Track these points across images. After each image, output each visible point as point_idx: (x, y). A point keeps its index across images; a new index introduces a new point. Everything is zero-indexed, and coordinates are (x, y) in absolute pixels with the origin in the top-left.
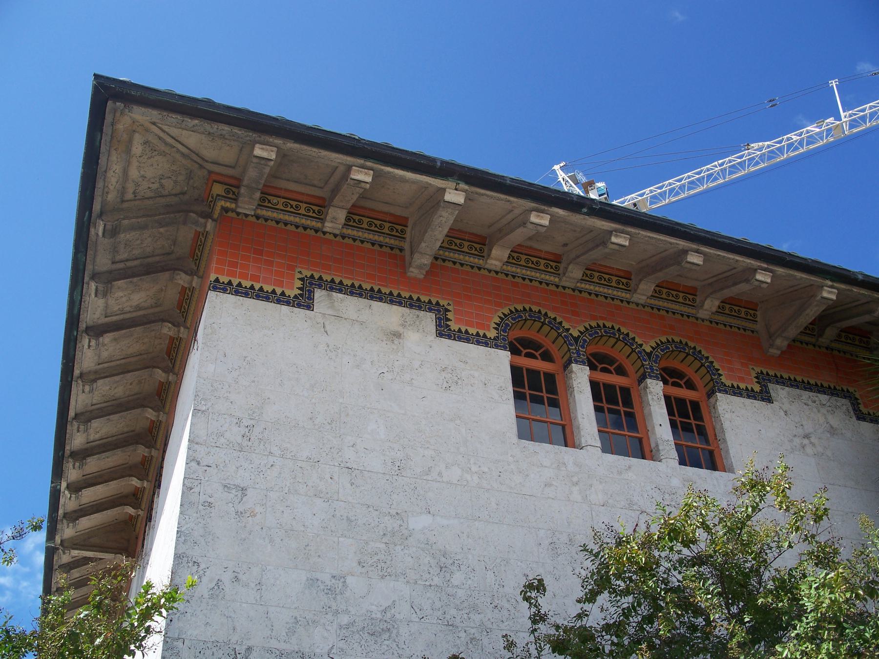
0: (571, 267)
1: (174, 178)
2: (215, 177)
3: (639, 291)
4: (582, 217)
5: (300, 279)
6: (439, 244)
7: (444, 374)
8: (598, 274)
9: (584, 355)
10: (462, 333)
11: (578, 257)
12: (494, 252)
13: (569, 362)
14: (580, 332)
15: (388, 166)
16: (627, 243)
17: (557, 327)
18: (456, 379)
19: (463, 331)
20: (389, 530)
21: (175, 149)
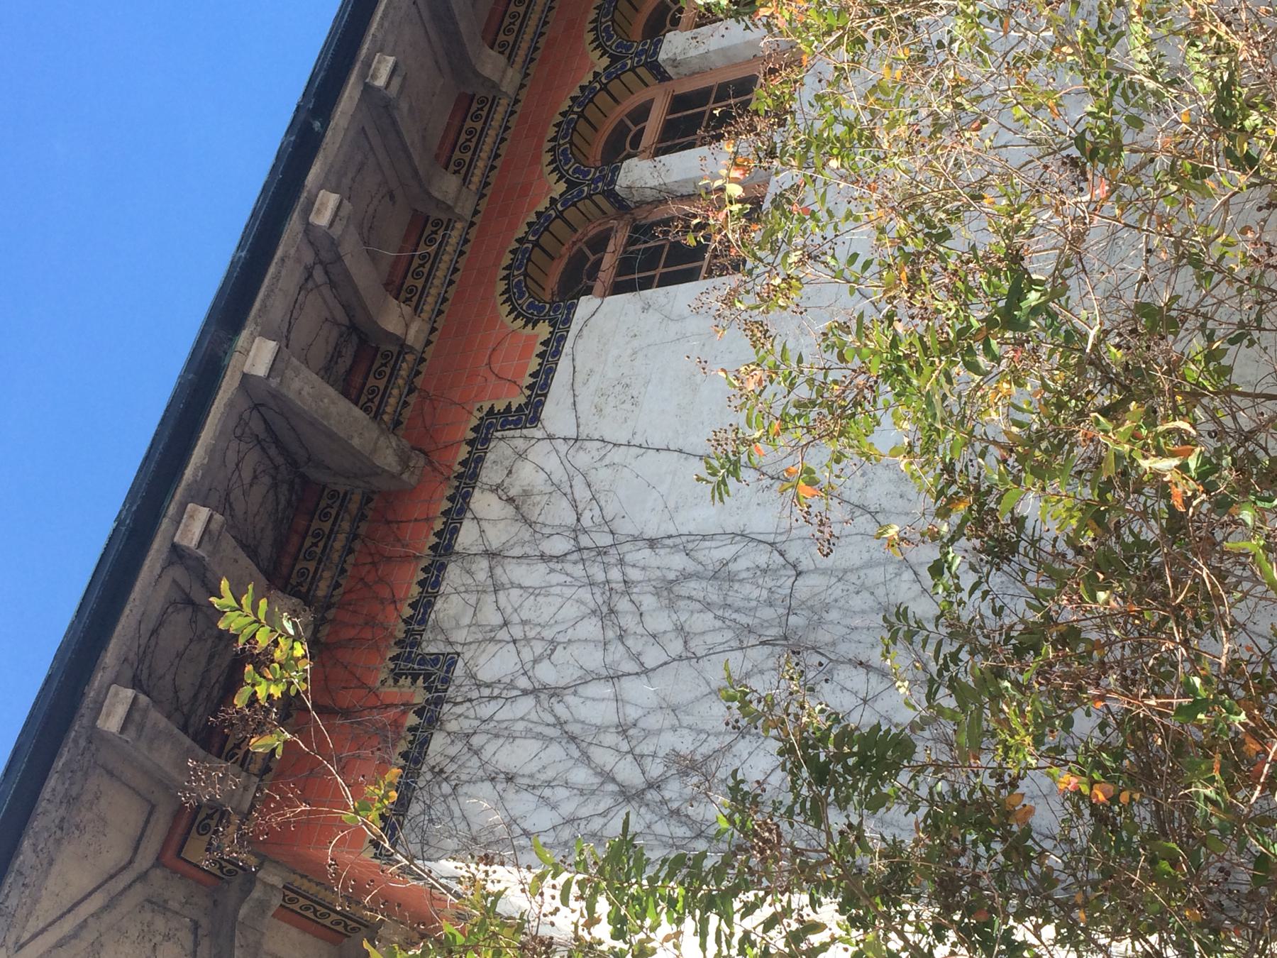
0: (436, 194)
1: (158, 938)
2: (170, 853)
3: (495, 78)
4: (329, 133)
5: (396, 681)
6: (357, 412)
7: (608, 410)
8: (457, 152)
10: (535, 383)
11: (416, 172)
12: (390, 328)
13: (611, 195)
15: (183, 474)
16: (391, 60)
17: (546, 220)
18: (619, 388)
19: (532, 380)
20: (893, 489)
21: (91, 920)
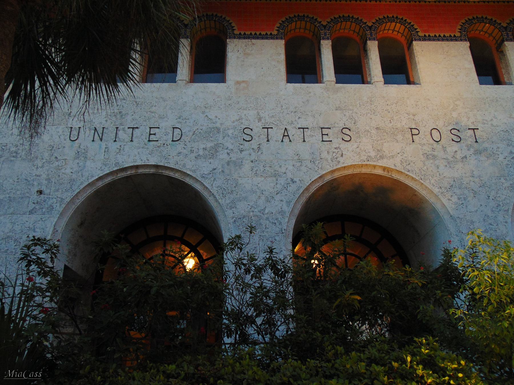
9: (328, 34)
14: (507, 23)
